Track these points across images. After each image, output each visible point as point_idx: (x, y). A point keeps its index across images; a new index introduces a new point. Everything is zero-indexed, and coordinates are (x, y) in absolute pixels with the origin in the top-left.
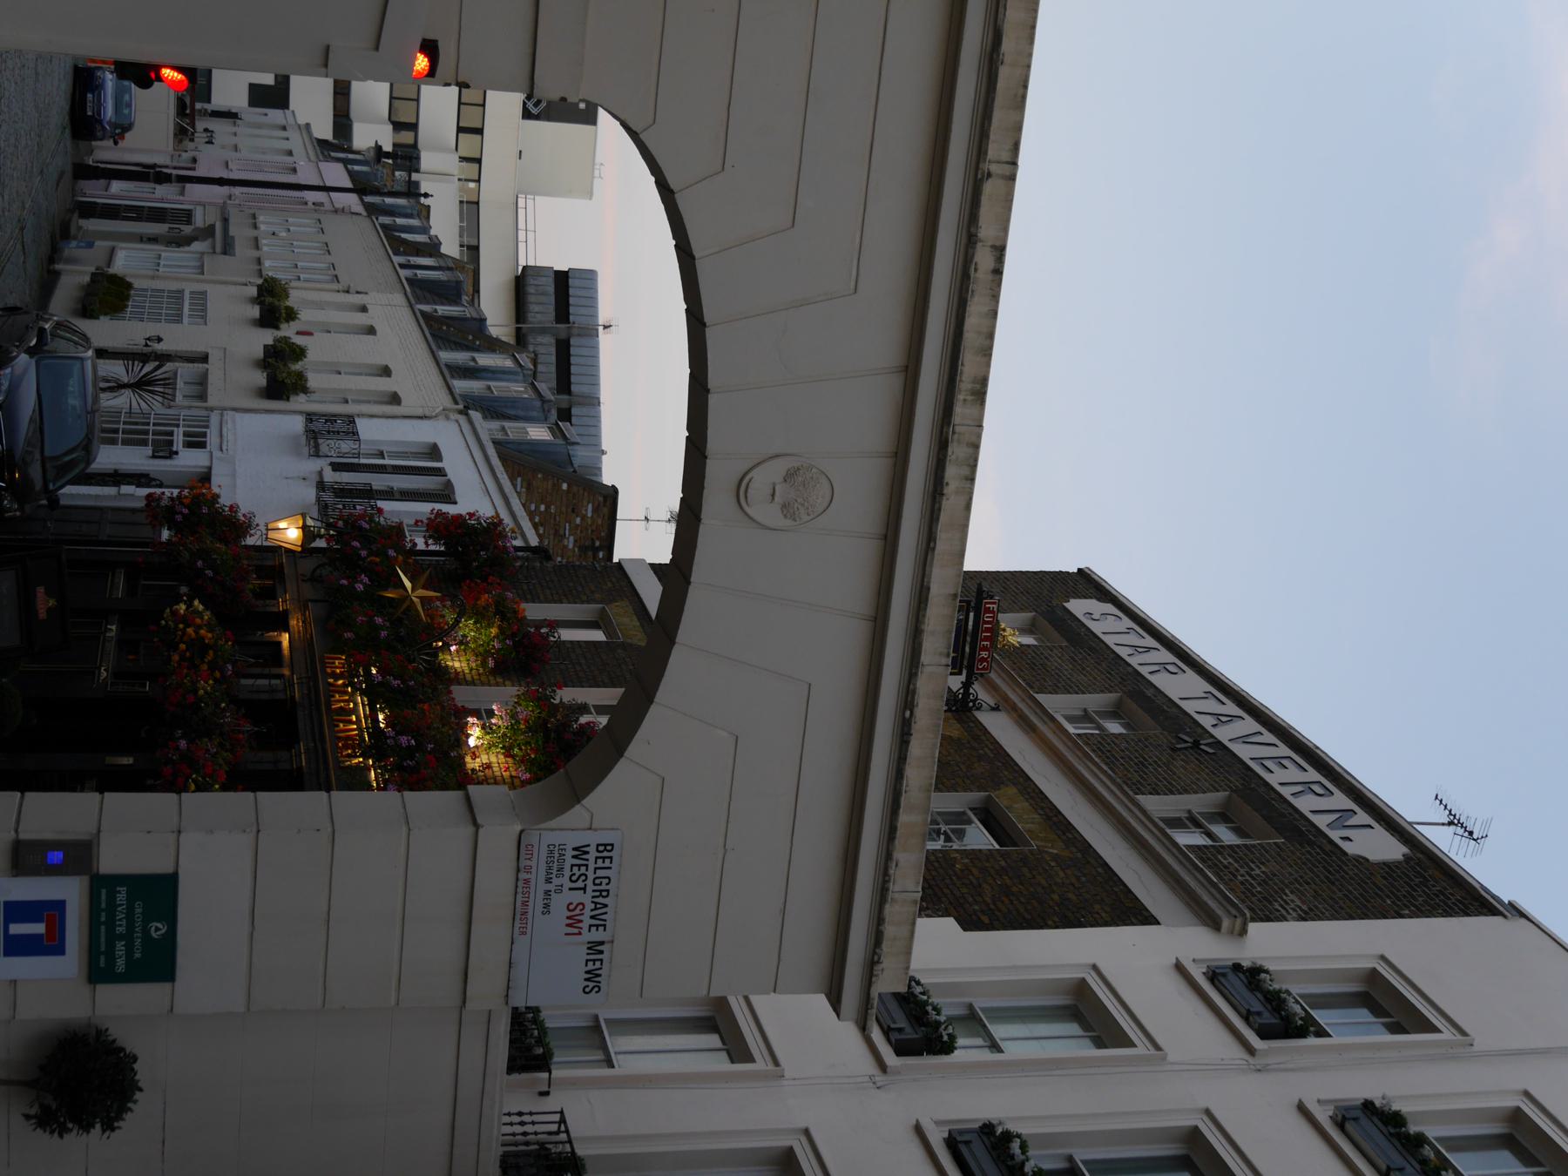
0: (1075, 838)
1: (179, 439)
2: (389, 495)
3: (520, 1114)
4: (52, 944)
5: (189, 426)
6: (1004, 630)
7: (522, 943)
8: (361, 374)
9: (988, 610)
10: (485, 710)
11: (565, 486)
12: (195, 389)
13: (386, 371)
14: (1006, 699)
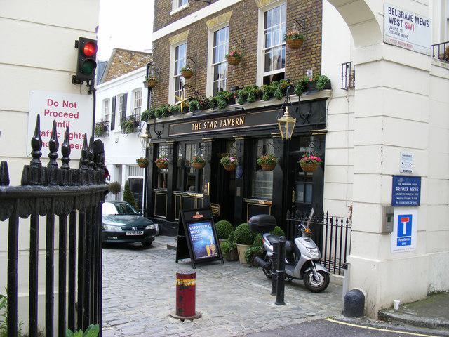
2: (124, 113)
3: (342, 76)
4: (408, 218)
7: (416, 48)
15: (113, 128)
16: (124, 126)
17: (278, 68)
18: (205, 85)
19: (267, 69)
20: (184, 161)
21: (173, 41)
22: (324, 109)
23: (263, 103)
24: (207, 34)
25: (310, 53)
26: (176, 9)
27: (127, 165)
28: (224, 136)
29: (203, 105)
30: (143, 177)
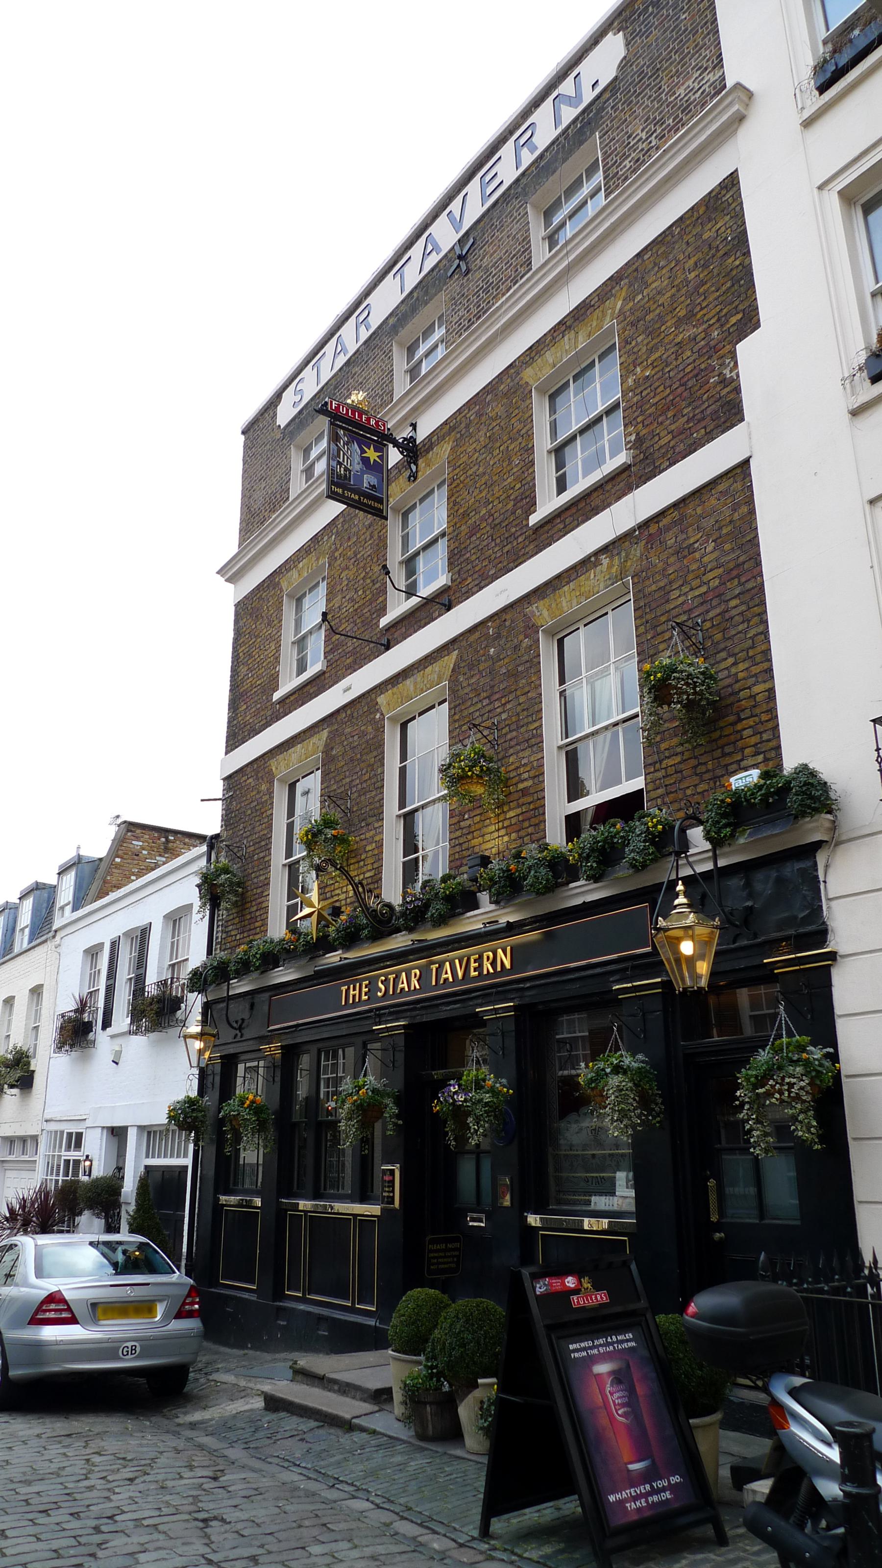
0: (598, 295)
1: (73, 1155)
2: (139, 981)
5: (60, 1147)
6: (353, 401)
8: (10, 1021)
9: (337, 408)
10: (404, 857)
11: (118, 860)
12: (18, 1146)
13: (9, 1002)
14: (405, 418)
15: (107, 1024)
16: (137, 1013)
17: (611, 780)
18: (378, 871)
19: (575, 789)
20: (314, 1102)
21: (281, 767)
22: (813, 884)
23: (284, 975)
24: (380, 730)
25: (732, 718)
26: (288, 684)
27: (141, 1128)
28: (445, 1012)
29: (380, 922)
30: (188, 1161)
